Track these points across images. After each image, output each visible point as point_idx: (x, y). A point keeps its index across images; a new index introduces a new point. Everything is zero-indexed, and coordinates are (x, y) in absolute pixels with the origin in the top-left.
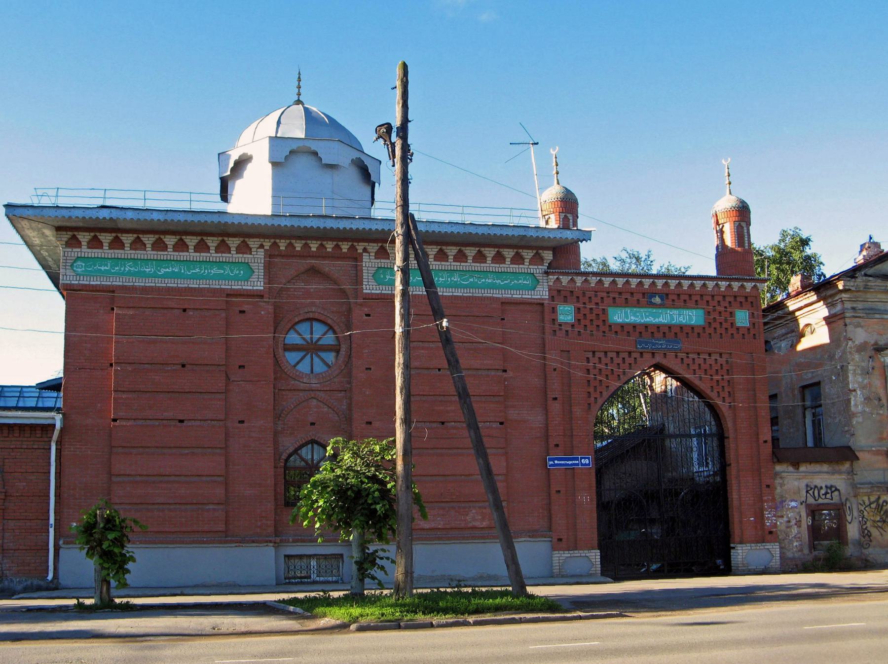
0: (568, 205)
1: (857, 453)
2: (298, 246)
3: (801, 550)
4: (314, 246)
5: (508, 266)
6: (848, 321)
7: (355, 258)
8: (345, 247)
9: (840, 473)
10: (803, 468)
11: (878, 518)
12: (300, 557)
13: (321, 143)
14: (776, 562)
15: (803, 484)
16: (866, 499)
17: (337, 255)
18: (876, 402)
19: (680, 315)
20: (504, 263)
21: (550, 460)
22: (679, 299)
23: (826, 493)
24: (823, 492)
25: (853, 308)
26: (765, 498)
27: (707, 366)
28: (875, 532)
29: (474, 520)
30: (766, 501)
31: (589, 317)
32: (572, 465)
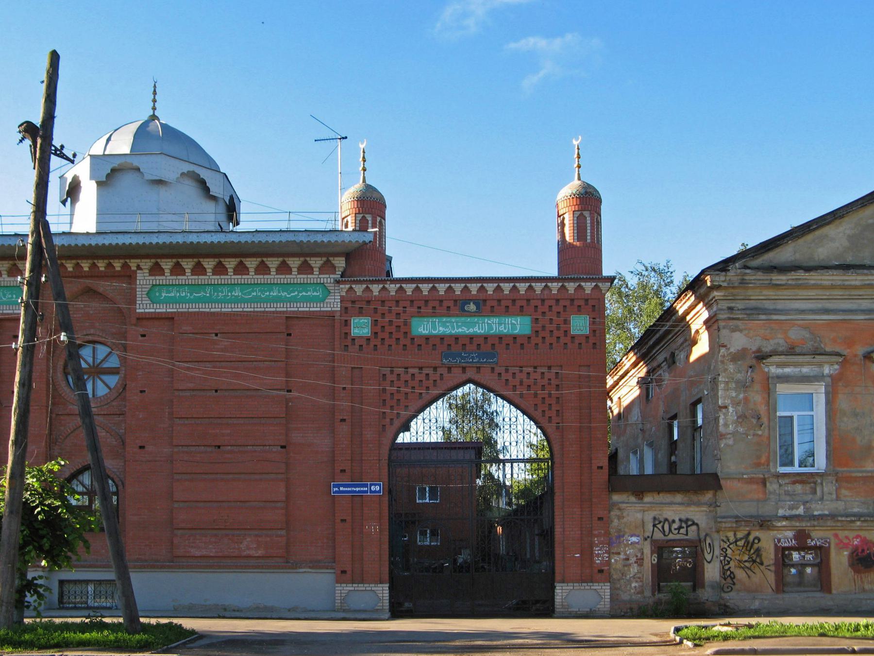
0: (371, 205)
1: (722, 482)
2: (86, 266)
3: (641, 592)
4: (86, 266)
5: (295, 277)
6: (722, 324)
7: (129, 276)
8: (117, 265)
9: (698, 504)
10: (648, 499)
11: (746, 558)
12: (75, 582)
13: (144, 158)
14: (605, 604)
15: (649, 517)
16: (731, 535)
17: (110, 275)
18: (754, 421)
19: (500, 324)
20: (291, 274)
21: (335, 486)
22: (441, 305)
23: (680, 528)
24: (675, 526)
25: (731, 309)
26: (596, 532)
27: (545, 382)
28: (740, 574)
29: (249, 549)
30: (597, 536)
31: (388, 329)
32: (359, 492)
